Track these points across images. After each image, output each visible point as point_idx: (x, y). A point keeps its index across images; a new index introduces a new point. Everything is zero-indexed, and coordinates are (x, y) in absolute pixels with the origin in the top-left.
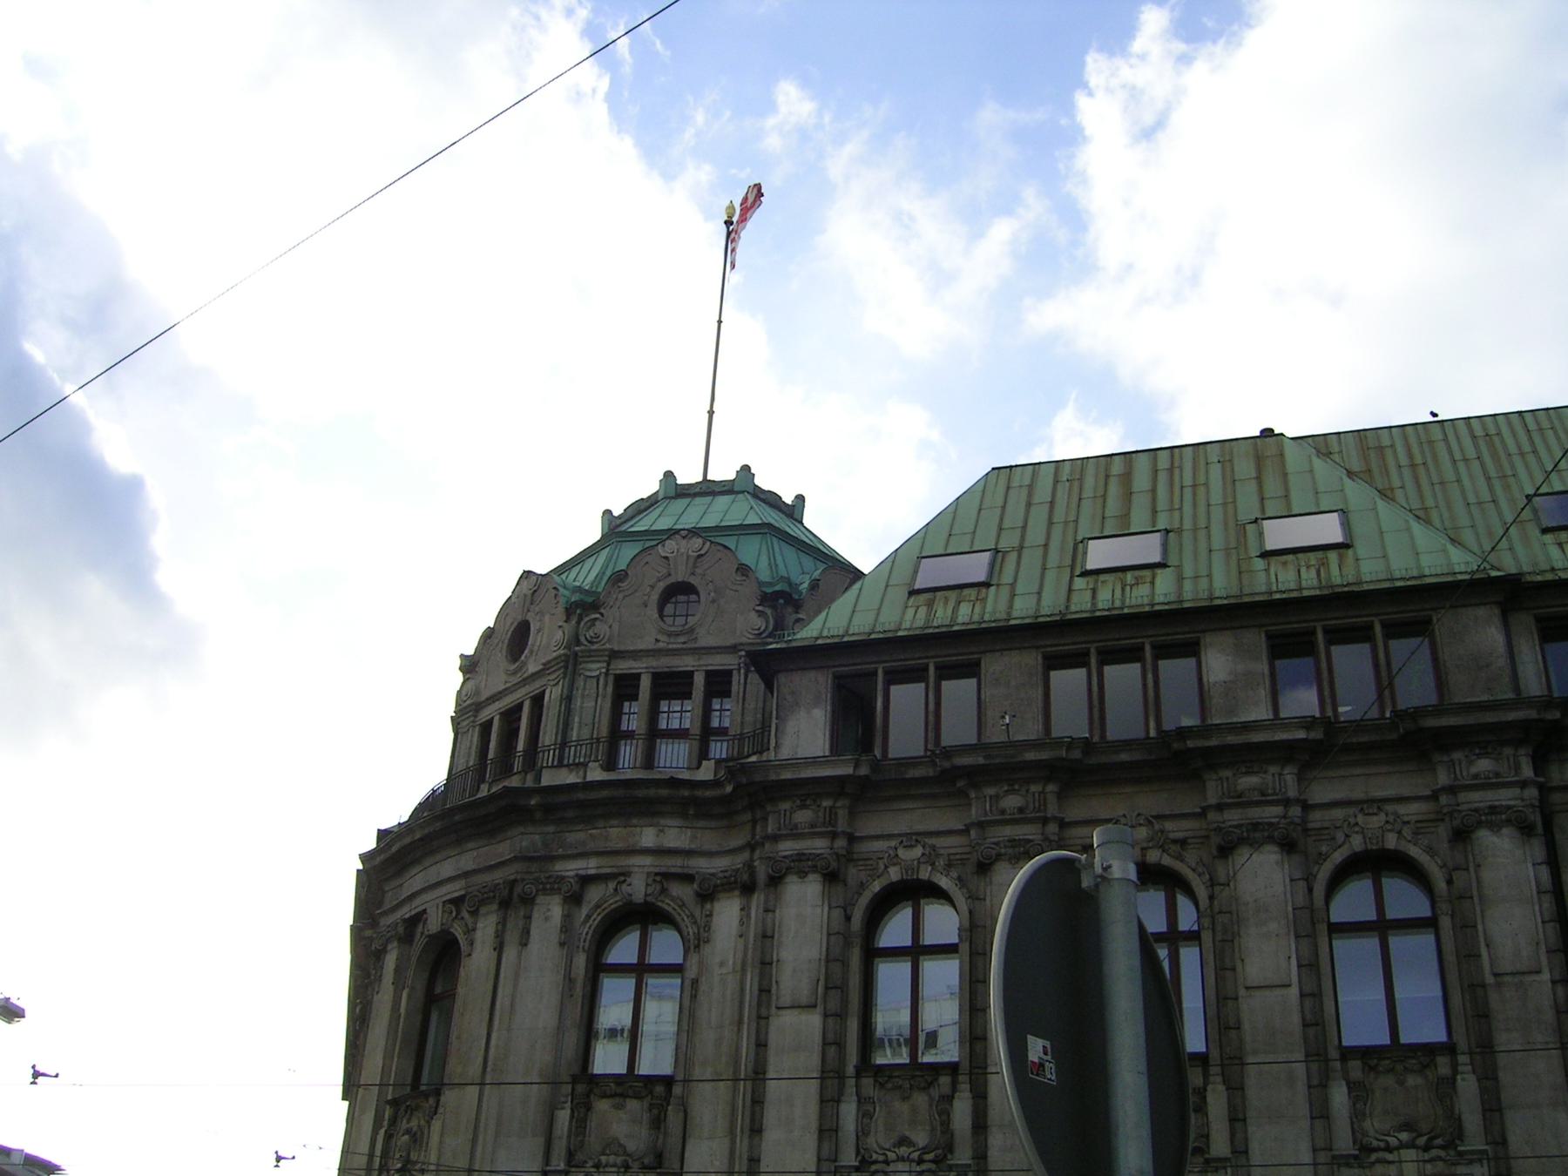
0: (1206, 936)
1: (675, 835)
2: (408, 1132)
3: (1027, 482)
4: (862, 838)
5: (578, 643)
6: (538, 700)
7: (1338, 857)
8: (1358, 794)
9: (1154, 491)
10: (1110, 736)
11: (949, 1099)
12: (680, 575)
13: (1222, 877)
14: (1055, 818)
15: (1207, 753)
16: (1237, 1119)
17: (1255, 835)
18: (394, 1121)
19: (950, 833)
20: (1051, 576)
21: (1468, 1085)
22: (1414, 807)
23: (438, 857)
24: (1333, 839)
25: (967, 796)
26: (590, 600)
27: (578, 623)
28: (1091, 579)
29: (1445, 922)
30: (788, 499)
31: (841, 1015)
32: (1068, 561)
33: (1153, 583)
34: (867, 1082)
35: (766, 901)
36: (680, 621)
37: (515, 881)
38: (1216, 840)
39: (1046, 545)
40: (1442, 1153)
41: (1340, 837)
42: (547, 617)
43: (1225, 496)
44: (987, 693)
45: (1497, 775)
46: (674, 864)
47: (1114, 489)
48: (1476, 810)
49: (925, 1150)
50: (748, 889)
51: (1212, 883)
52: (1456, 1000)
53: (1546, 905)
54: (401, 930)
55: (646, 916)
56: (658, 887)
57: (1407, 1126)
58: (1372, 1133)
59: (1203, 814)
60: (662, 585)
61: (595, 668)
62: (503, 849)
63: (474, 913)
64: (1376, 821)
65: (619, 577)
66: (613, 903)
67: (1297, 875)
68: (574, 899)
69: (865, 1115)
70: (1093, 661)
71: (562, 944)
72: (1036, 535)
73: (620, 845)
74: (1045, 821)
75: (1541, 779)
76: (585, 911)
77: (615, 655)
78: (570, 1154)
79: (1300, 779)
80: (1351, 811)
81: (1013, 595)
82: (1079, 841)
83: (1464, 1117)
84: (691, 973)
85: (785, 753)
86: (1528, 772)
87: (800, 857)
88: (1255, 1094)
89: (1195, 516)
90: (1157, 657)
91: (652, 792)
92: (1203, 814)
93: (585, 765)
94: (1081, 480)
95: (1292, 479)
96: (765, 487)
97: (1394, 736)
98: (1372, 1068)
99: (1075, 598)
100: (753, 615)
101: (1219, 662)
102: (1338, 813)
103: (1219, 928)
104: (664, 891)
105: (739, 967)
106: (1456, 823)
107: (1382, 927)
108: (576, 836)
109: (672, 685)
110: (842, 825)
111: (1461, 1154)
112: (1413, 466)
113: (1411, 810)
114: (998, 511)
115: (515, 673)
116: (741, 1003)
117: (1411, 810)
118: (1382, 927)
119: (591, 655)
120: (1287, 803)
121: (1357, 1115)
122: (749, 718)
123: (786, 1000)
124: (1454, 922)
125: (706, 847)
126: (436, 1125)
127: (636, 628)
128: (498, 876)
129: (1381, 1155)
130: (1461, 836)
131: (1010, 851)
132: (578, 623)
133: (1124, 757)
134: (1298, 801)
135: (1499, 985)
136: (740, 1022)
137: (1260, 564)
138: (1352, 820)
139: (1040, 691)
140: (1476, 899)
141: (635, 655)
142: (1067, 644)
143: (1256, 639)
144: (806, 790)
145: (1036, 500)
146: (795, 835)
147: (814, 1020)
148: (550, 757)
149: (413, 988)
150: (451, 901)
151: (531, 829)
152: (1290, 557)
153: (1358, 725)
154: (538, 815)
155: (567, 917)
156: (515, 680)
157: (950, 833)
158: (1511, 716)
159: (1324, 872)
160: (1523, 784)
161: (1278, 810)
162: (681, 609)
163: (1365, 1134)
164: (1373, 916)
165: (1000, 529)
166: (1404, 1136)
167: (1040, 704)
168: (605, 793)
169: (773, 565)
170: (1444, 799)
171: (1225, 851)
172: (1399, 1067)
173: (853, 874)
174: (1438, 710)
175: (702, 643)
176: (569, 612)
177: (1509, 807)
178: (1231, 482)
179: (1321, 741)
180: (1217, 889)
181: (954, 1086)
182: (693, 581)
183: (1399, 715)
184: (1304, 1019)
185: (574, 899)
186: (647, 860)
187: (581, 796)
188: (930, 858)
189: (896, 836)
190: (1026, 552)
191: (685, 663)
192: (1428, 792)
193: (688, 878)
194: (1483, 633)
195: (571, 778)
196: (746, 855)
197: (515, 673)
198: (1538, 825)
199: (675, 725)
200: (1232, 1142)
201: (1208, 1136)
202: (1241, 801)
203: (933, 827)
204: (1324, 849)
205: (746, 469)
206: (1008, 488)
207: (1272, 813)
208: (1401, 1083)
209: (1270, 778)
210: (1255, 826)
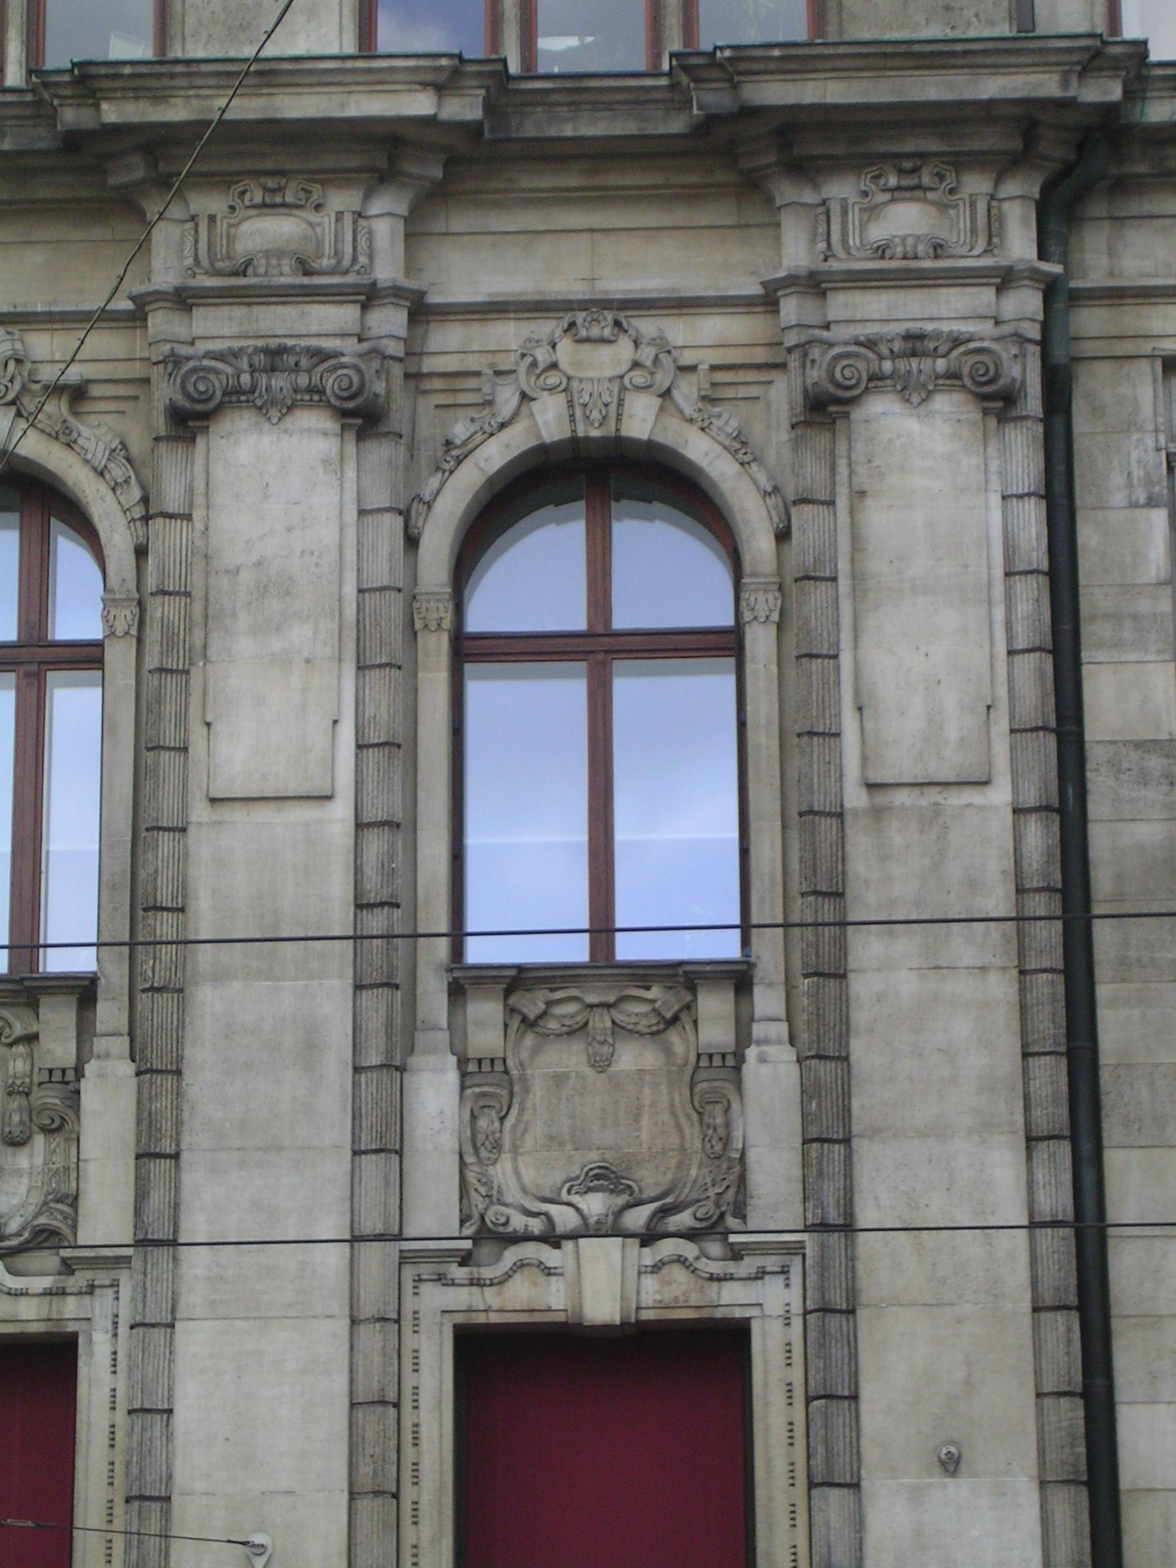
0: (120, 657)
4: (448, 312)
7: (496, 455)
8: (566, 283)
11: (731, 1063)
13: (172, 497)
15: (158, 142)
16: (156, 1152)
21: (772, 1077)
24: (489, 403)
25: (138, 214)
29: (760, 642)
38: (165, 391)
40: (689, 1249)
41: (507, 398)
45: (938, 250)
48: (870, 344)
51: (149, 511)
52: (767, 851)
53: (1023, 608)
57: (604, 1177)
58: (513, 1194)
64: (608, 361)
67: (379, 497)
75: (1056, 269)
79: (414, 233)
80: (546, 327)
83: (752, 1156)
86: (1020, 245)
88: (210, 1087)
92: (137, 317)
97: (677, 125)
98: (529, 1024)
102: (507, 334)
103: (153, 635)
106: (815, 374)
107: (599, 650)
111: (735, 1253)
113: (706, 336)
117: (706, 336)
118: (599, 650)
120: (369, 296)
121: (477, 1148)
124: (783, 650)
129: (530, 1251)
130: (824, 410)
134: (397, 293)
135: (877, 813)
138: (542, 355)
140: (844, 583)
153: (577, 89)
158: (992, 87)
159: (453, 499)
160: (1005, 280)
161: (344, 315)
163: (494, 1197)
164: (577, 621)
166: (595, 1205)
170: (791, 308)
171: (188, 422)
172: (601, 1022)
174: (793, 60)
177: (957, 341)
179: (472, 130)
183: (696, 66)
184: (358, 894)
192: (756, 290)
198: (1042, 400)
200: (138, 1211)
201: (74, 1201)
202: (241, 287)
204: (460, 430)
207: (325, 322)
208: (600, 1064)
210: (275, 357)
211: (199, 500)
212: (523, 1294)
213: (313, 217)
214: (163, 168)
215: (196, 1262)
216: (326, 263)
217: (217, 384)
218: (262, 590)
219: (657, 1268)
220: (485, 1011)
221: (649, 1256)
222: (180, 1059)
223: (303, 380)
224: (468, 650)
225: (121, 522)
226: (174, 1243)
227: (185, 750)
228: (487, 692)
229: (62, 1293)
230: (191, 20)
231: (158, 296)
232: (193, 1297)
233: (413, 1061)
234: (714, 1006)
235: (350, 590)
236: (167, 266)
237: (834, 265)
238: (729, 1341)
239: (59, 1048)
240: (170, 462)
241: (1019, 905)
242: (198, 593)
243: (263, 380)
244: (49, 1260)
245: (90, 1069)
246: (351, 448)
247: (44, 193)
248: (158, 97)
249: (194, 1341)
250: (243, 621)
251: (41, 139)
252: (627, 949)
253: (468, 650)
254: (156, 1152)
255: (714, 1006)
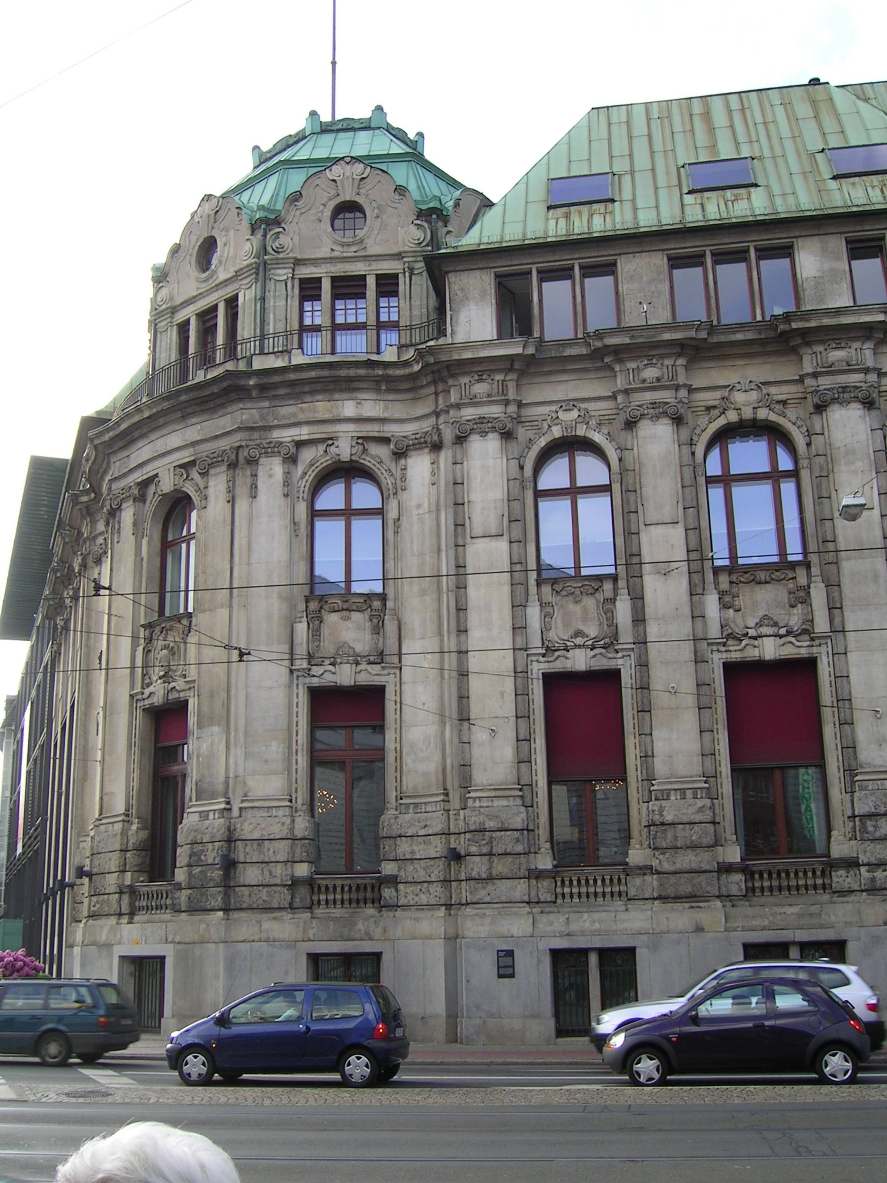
1: (370, 406)
2: (165, 647)
3: (624, 119)
5: (266, 252)
6: (232, 303)
7: (543, 442)
9: (732, 126)
10: (724, 322)
11: (613, 601)
12: (348, 195)
14: (685, 385)
15: (804, 333)
16: (834, 607)
17: (843, 396)
18: (149, 640)
19: (599, 399)
20: (663, 193)
22: (786, 389)
23: (164, 431)
26: (273, 217)
27: (265, 236)
28: (698, 195)
29: (616, 487)
30: (412, 135)
31: (522, 542)
32: (675, 182)
33: (749, 198)
34: (546, 589)
35: (454, 456)
36: (349, 233)
37: (239, 447)
38: (622, 417)
39: (653, 170)
40: (603, 651)
42: (232, 233)
43: (792, 132)
44: (624, 287)
46: (373, 430)
47: (698, 125)
49: (596, 639)
50: (437, 447)
54: (135, 491)
55: (348, 471)
56: (361, 448)
59: (801, 380)
60: (332, 204)
61: (283, 273)
62: (224, 422)
63: (204, 474)
65: (295, 197)
66: (325, 462)
68: (292, 460)
69: (547, 616)
70: (709, 260)
71: (286, 496)
72: (642, 161)
73: (327, 416)
74: (677, 388)
76: (300, 469)
77: (298, 262)
78: (310, 657)
81: (635, 209)
82: (703, 404)
84: (392, 513)
85: (460, 338)
87: (482, 420)
89: (771, 147)
90: (584, 276)
91: (352, 372)
92: (801, 380)
93: (289, 352)
94: (669, 117)
95: (844, 118)
96: (395, 125)
99: (688, 210)
100: (413, 228)
101: (811, 260)
104: (365, 450)
105: (433, 508)
107: (574, 492)
108: (288, 410)
109: (348, 287)
110: (512, 395)
112: (765, 123)
114: (606, 143)
115: (206, 280)
116: (439, 536)
119: (278, 263)
120: (867, 371)
122: (416, 312)
123: (478, 531)
125: (397, 415)
126: (192, 638)
127: (311, 239)
128: (224, 444)
131: (652, 411)
132: (265, 236)
133: (739, 336)
136: (439, 550)
137: (833, 185)
139: (667, 283)
141: (315, 262)
142: (689, 246)
143: (839, 244)
144: (481, 367)
145: (635, 133)
146: (474, 402)
147: (503, 545)
148: (253, 347)
149: (151, 537)
150: (181, 466)
151: (249, 405)
152: (857, 179)
154: (254, 394)
155: (287, 474)
156: (204, 287)
157: (599, 399)
161: (860, 377)
162: (349, 223)
165: (611, 157)
167: (668, 296)
168: (313, 374)
169: (421, 187)
171: (820, 408)
173: (522, 433)
174: (612, 332)
175: (373, 250)
176: (253, 228)
178: (793, 119)
180: (813, 437)
181: (615, 590)
182: (360, 200)
185: (292, 460)
186: (351, 427)
187: (292, 376)
188: (585, 418)
189: (560, 401)
190: (637, 175)
191: (358, 268)
193: (386, 440)
194: (641, 272)
195: (279, 363)
196: (432, 421)
197: (206, 280)
199: (351, 319)
202: (831, 371)
203: (586, 394)
205: (379, 108)
206: (609, 124)
207: (855, 378)
209: (853, 351)
210: (844, 389)
211: (826, 429)
212: (559, 665)
213: (849, 350)
214: (807, 339)
215: (851, 636)
216: (854, 362)
217: (828, 398)
218: (847, 453)
219: (594, 656)
220: (546, 589)
221: (592, 653)
222: (840, 581)
223: (852, 395)
224: (539, 494)
225: (801, 437)
226: (844, 631)
227: (829, 497)
228: (545, 505)
229: (812, 646)
230: (806, 300)
231: (808, 374)
232: (851, 646)
233: (529, 604)
234: (608, 586)
235: (871, 451)
236: (808, 367)
237: (463, 401)
238: (614, 675)
239: (802, 580)
240: (816, 419)
241: (457, 571)
242: (829, 455)
243: (841, 395)
244: (806, 637)
245: (812, 585)
246: (867, 412)
247: (769, 349)
248: (807, 320)
249: (852, 657)
250: (843, 462)
251: (771, 334)
252: (584, 572)
253: (539, 494)
254: (834, 607)
255: (608, 586)
